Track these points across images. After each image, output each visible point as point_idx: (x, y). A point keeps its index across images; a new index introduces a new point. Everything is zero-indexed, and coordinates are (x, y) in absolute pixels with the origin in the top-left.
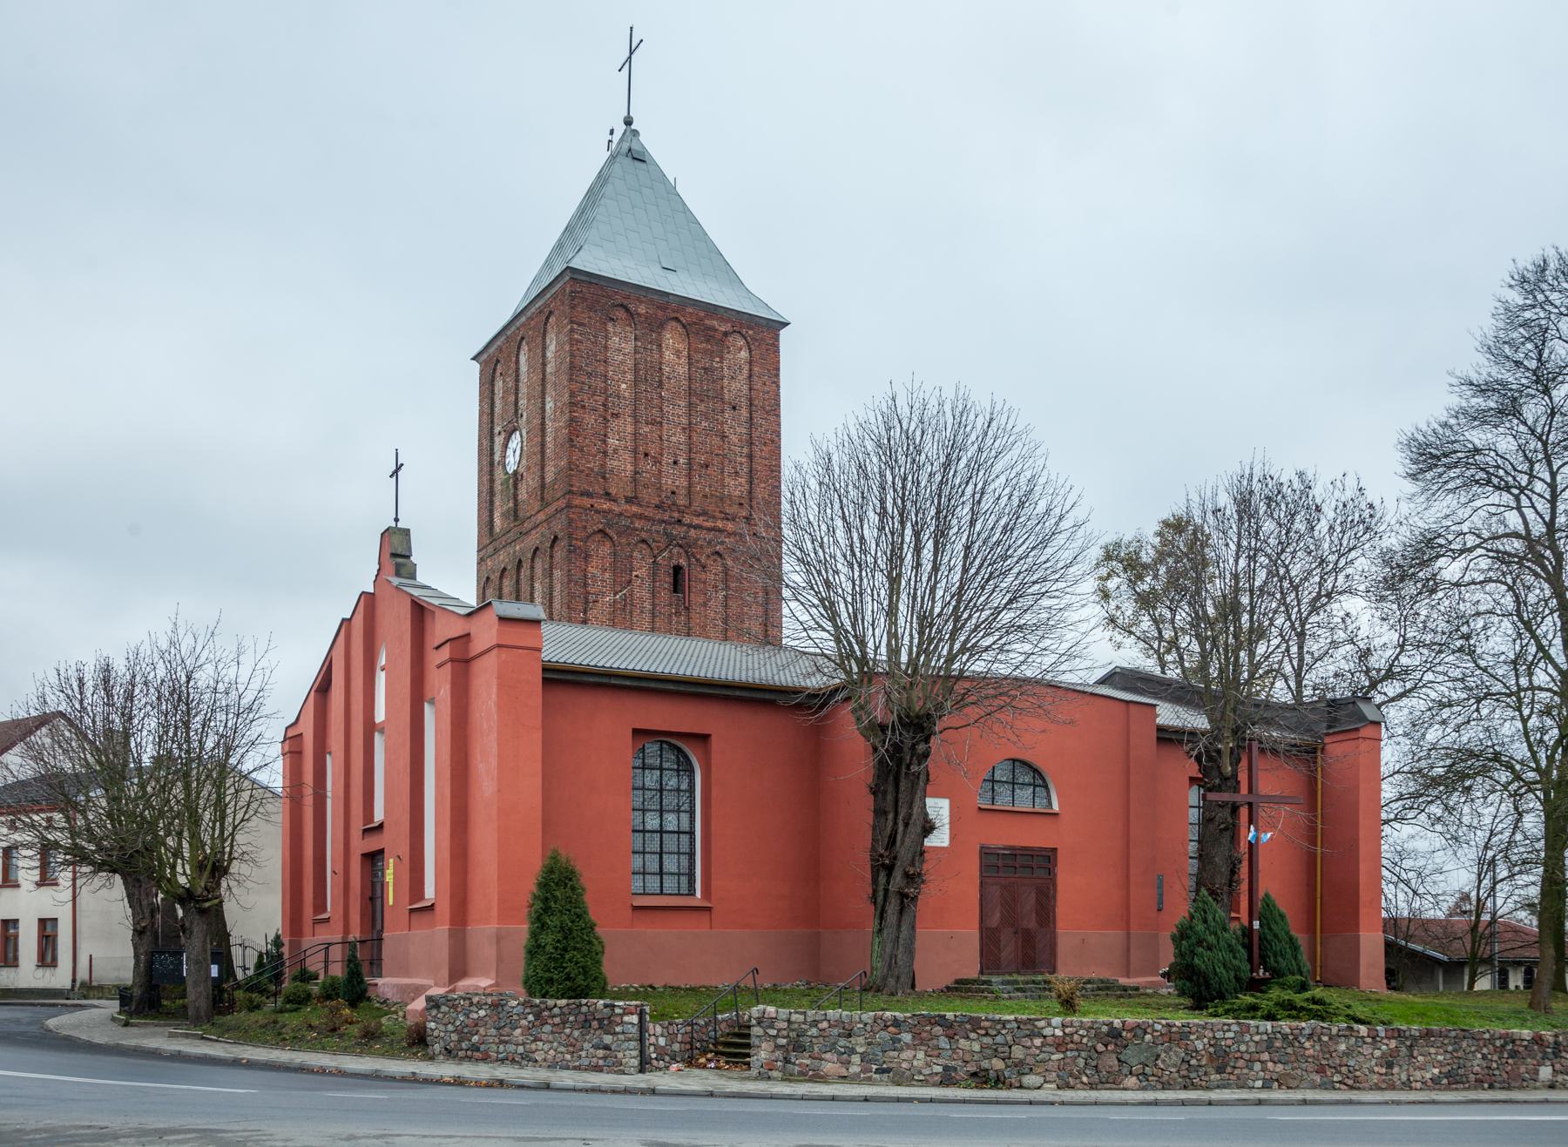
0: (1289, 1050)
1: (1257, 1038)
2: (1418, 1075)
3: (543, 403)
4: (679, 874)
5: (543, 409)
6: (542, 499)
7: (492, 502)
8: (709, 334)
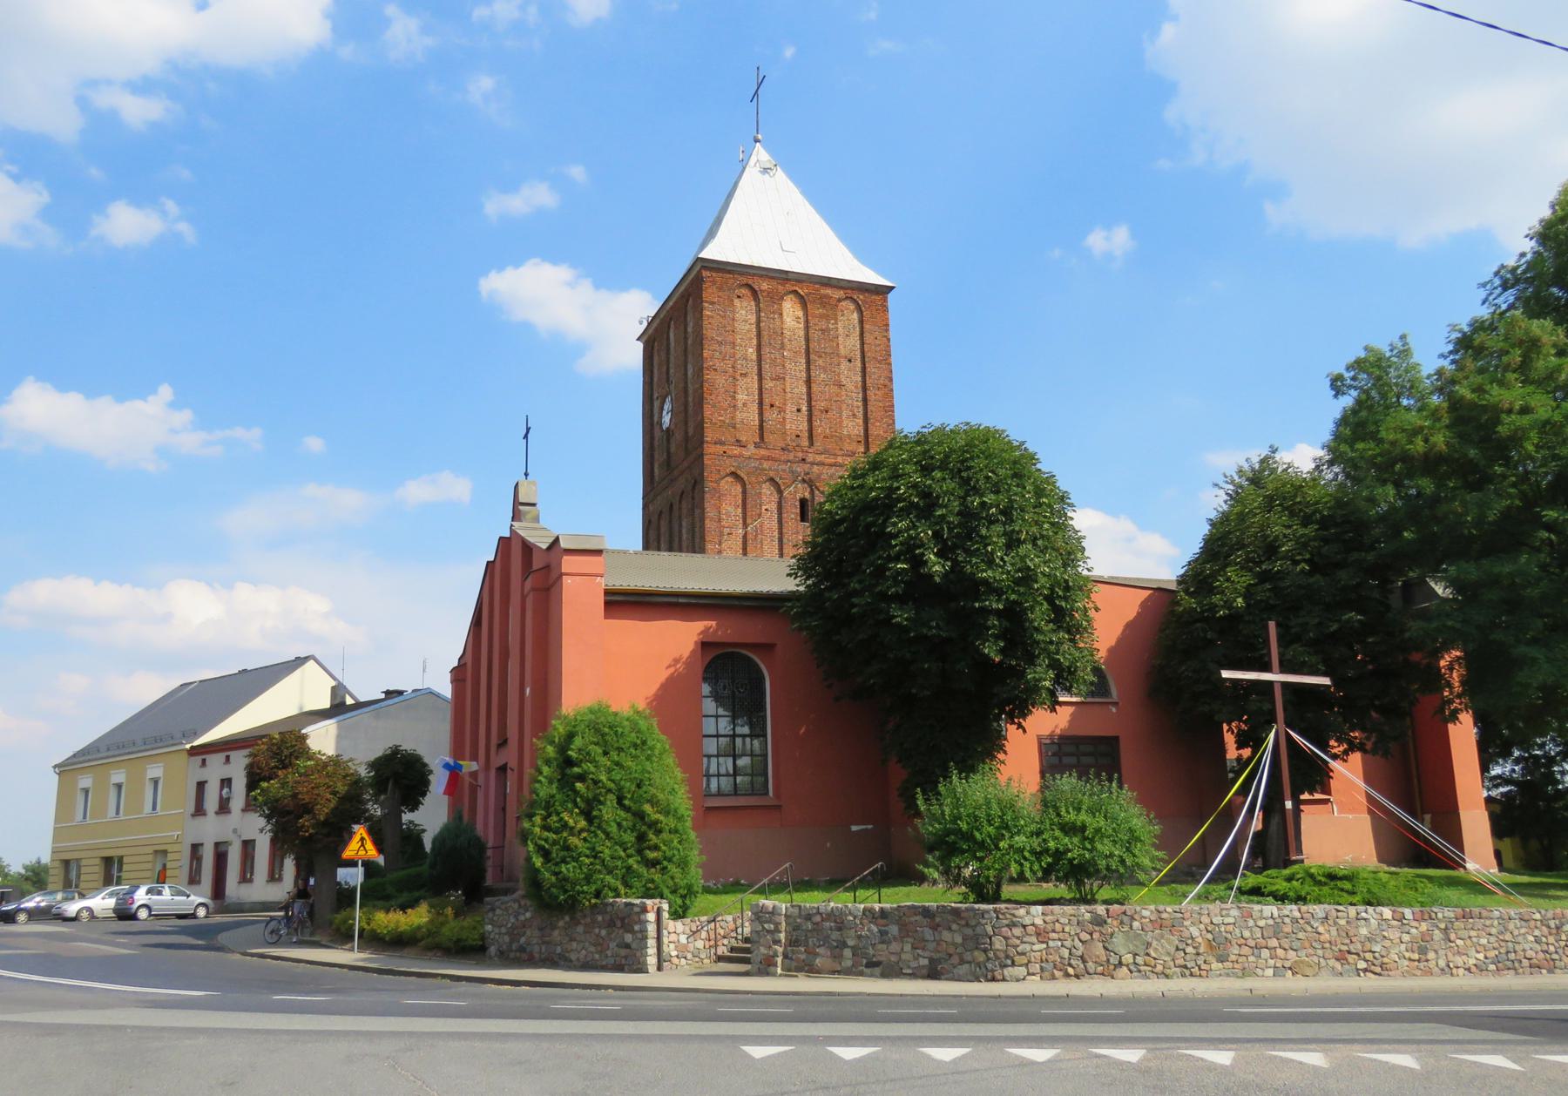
0: (1301, 935)
1: (1262, 923)
2: (1459, 960)
7: (652, 456)
8: (824, 301)
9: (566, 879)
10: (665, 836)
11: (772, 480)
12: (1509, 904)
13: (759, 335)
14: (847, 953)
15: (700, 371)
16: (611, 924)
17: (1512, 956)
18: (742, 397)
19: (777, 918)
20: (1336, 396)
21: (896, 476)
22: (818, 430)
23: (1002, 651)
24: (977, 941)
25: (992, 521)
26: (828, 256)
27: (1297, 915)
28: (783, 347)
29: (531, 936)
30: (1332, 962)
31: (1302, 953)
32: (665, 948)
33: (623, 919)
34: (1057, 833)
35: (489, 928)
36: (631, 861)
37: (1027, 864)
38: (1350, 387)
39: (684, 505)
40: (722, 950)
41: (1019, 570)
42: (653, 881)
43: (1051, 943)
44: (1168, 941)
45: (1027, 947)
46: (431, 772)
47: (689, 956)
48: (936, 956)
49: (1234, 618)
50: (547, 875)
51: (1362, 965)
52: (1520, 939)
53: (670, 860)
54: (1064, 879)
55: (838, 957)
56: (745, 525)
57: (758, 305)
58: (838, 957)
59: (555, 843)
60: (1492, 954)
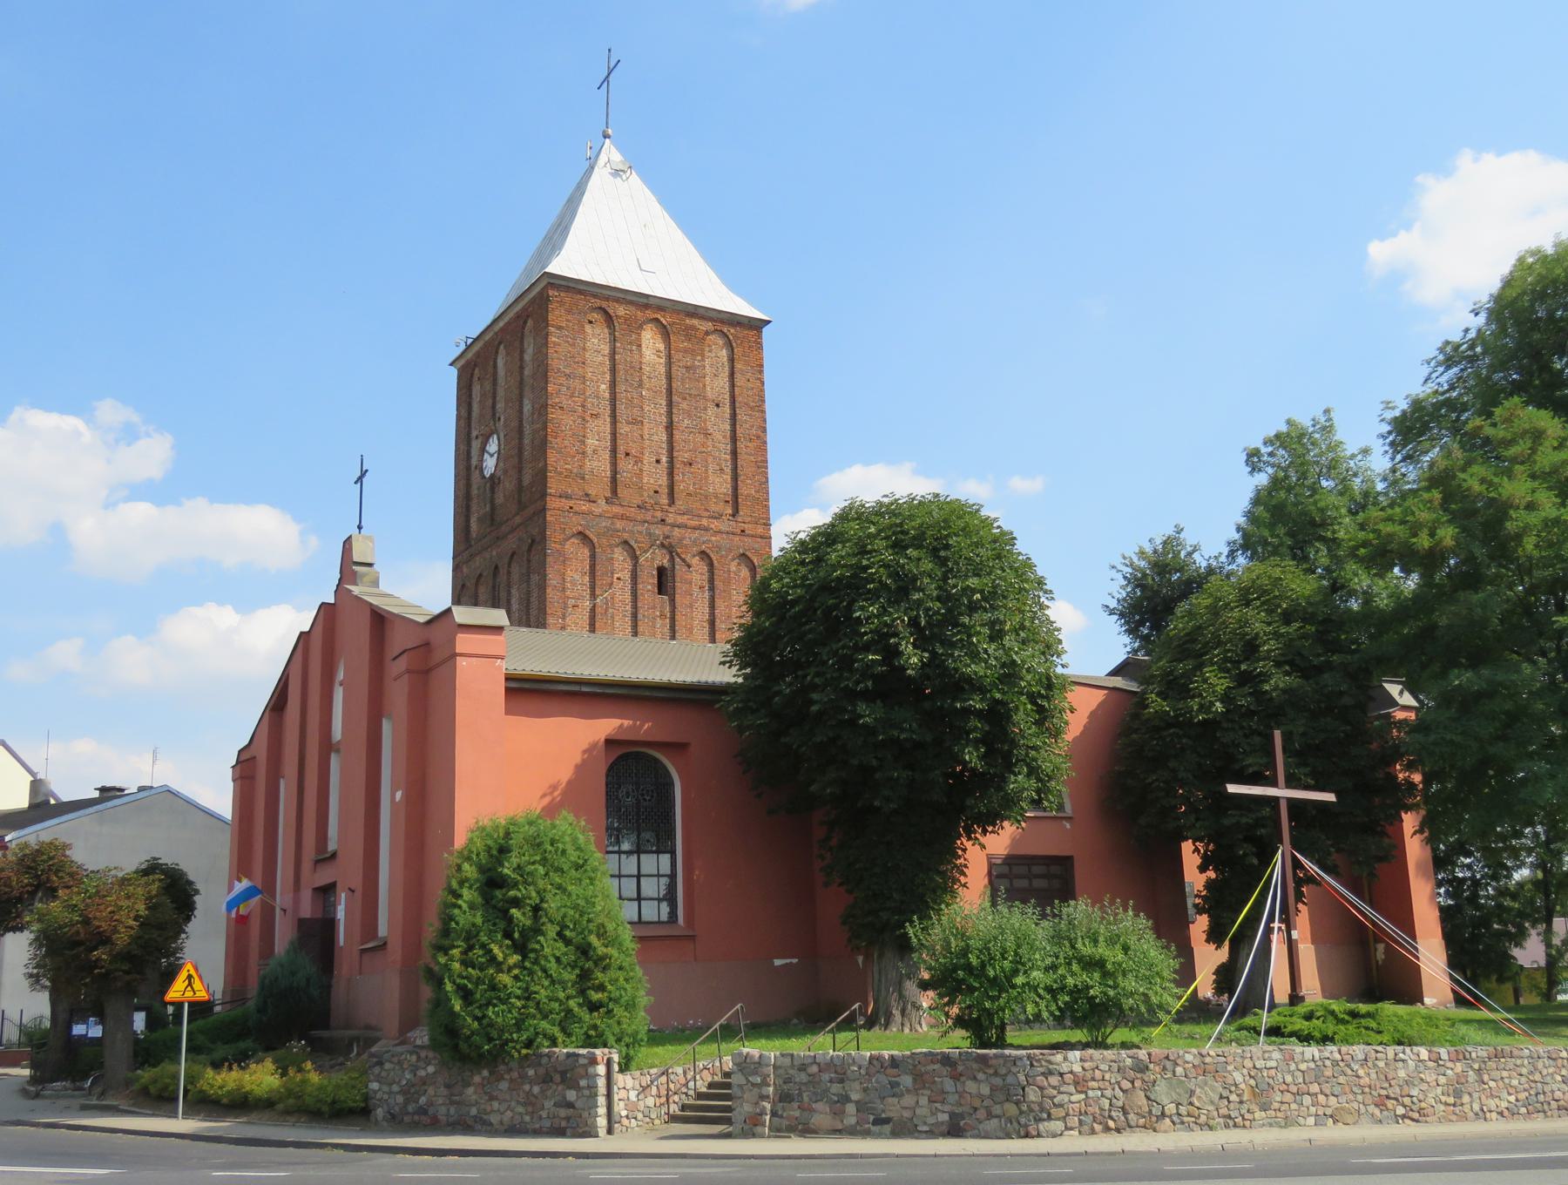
0: (1342, 1079)
1: (1303, 1067)
2: (1492, 1103)
3: (521, 406)
4: (659, 900)
5: (521, 411)
6: (520, 502)
7: (468, 508)
8: (689, 333)
9: (491, 1025)
10: (612, 974)
11: (626, 542)
12: (1536, 1043)
13: (613, 370)
14: (851, 1108)
15: (542, 409)
16: (546, 1080)
17: (1541, 1098)
18: (591, 442)
19: (765, 1070)
20: (1251, 473)
21: (863, 552)
22: (680, 487)
23: (981, 758)
24: (1009, 1093)
25: (973, 608)
26: (688, 278)
27: (1338, 1057)
28: (641, 385)
29: (435, 1096)
30: (1372, 1109)
31: (1343, 1099)
32: (616, 1109)
33: (563, 1073)
34: (1075, 967)
35: (375, 1086)
36: (572, 1003)
37: (1043, 1005)
38: (1267, 463)
39: (515, 569)
40: (674, 1109)
41: (1003, 665)
42: (595, 1027)
43: (1090, 1093)
44: (1213, 1089)
45: (1065, 1098)
46: (197, 892)
47: (640, 1116)
48: (958, 1110)
49: (1210, 726)
50: (469, 1020)
51: (1400, 1111)
52: (1548, 1079)
53: (616, 1001)
54: (1078, 1023)
55: (838, 1113)
56: (593, 596)
57: (613, 333)
58: (838, 1113)
59: (479, 981)
60: (1522, 1096)
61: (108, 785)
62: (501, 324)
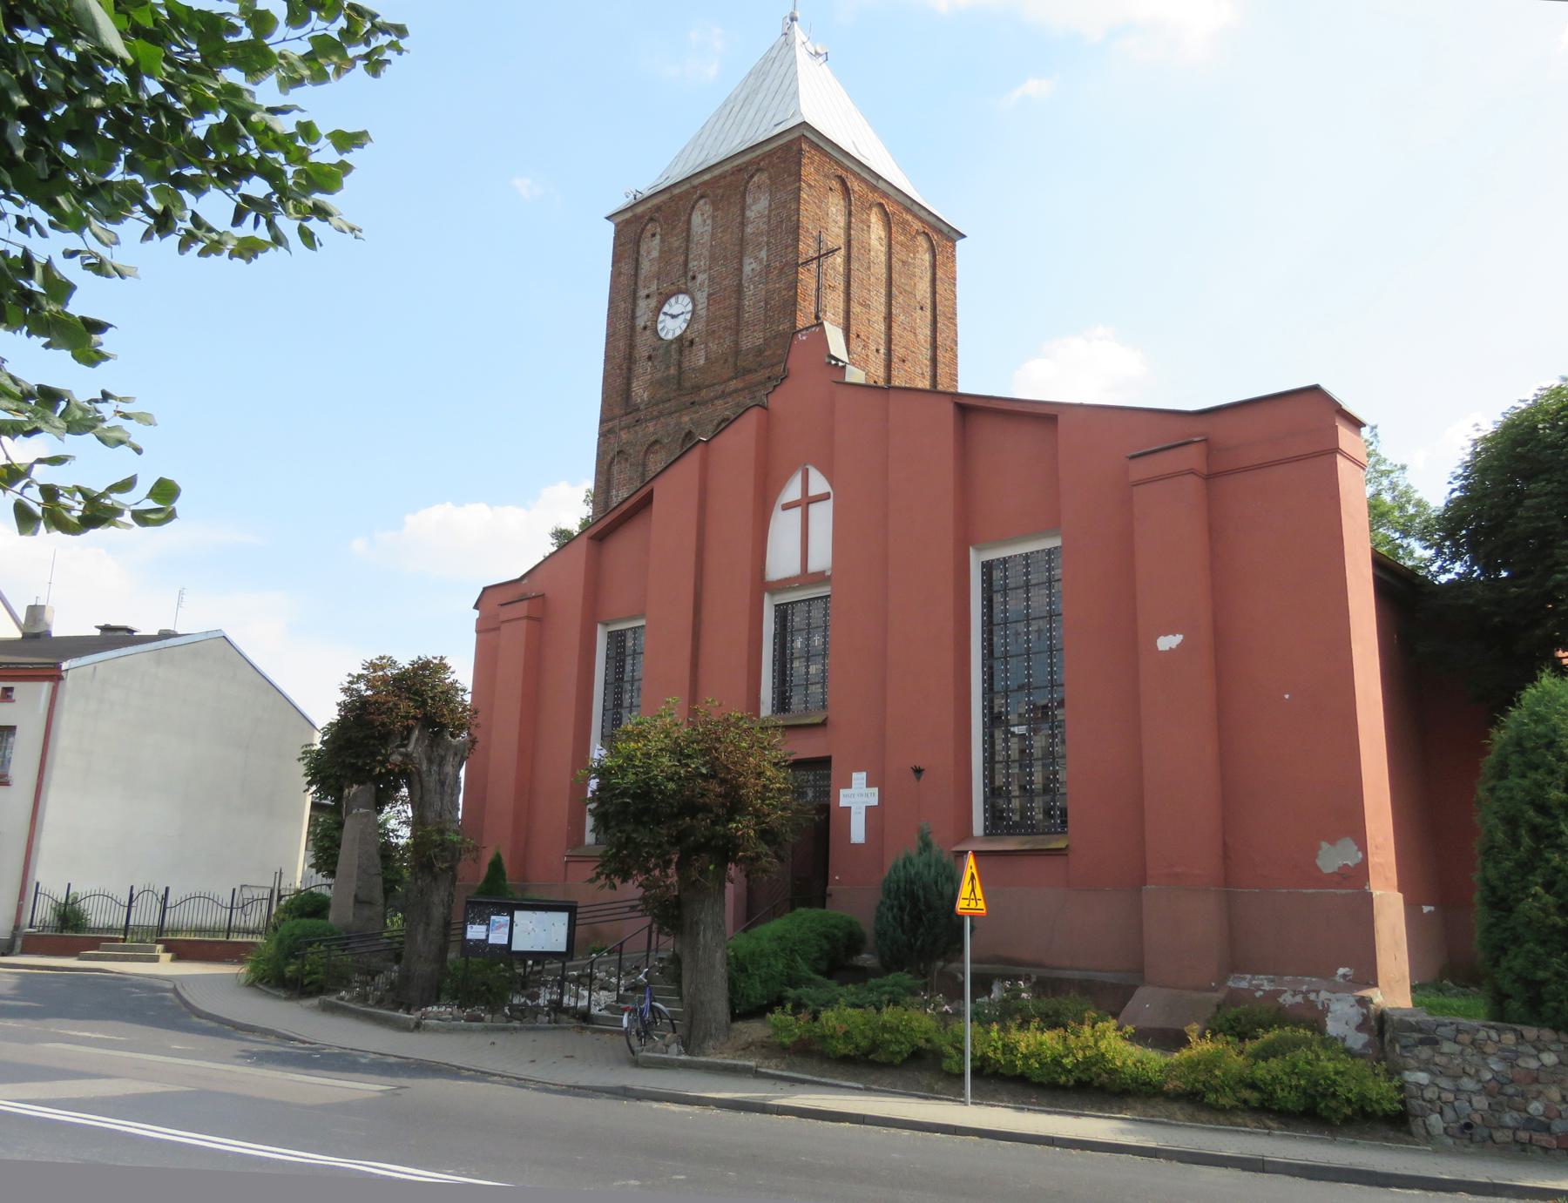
61: (113, 623)
62: (706, 177)
